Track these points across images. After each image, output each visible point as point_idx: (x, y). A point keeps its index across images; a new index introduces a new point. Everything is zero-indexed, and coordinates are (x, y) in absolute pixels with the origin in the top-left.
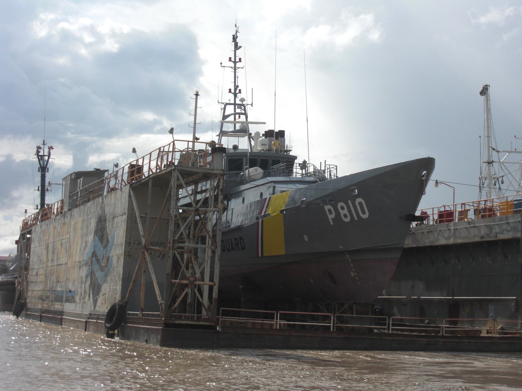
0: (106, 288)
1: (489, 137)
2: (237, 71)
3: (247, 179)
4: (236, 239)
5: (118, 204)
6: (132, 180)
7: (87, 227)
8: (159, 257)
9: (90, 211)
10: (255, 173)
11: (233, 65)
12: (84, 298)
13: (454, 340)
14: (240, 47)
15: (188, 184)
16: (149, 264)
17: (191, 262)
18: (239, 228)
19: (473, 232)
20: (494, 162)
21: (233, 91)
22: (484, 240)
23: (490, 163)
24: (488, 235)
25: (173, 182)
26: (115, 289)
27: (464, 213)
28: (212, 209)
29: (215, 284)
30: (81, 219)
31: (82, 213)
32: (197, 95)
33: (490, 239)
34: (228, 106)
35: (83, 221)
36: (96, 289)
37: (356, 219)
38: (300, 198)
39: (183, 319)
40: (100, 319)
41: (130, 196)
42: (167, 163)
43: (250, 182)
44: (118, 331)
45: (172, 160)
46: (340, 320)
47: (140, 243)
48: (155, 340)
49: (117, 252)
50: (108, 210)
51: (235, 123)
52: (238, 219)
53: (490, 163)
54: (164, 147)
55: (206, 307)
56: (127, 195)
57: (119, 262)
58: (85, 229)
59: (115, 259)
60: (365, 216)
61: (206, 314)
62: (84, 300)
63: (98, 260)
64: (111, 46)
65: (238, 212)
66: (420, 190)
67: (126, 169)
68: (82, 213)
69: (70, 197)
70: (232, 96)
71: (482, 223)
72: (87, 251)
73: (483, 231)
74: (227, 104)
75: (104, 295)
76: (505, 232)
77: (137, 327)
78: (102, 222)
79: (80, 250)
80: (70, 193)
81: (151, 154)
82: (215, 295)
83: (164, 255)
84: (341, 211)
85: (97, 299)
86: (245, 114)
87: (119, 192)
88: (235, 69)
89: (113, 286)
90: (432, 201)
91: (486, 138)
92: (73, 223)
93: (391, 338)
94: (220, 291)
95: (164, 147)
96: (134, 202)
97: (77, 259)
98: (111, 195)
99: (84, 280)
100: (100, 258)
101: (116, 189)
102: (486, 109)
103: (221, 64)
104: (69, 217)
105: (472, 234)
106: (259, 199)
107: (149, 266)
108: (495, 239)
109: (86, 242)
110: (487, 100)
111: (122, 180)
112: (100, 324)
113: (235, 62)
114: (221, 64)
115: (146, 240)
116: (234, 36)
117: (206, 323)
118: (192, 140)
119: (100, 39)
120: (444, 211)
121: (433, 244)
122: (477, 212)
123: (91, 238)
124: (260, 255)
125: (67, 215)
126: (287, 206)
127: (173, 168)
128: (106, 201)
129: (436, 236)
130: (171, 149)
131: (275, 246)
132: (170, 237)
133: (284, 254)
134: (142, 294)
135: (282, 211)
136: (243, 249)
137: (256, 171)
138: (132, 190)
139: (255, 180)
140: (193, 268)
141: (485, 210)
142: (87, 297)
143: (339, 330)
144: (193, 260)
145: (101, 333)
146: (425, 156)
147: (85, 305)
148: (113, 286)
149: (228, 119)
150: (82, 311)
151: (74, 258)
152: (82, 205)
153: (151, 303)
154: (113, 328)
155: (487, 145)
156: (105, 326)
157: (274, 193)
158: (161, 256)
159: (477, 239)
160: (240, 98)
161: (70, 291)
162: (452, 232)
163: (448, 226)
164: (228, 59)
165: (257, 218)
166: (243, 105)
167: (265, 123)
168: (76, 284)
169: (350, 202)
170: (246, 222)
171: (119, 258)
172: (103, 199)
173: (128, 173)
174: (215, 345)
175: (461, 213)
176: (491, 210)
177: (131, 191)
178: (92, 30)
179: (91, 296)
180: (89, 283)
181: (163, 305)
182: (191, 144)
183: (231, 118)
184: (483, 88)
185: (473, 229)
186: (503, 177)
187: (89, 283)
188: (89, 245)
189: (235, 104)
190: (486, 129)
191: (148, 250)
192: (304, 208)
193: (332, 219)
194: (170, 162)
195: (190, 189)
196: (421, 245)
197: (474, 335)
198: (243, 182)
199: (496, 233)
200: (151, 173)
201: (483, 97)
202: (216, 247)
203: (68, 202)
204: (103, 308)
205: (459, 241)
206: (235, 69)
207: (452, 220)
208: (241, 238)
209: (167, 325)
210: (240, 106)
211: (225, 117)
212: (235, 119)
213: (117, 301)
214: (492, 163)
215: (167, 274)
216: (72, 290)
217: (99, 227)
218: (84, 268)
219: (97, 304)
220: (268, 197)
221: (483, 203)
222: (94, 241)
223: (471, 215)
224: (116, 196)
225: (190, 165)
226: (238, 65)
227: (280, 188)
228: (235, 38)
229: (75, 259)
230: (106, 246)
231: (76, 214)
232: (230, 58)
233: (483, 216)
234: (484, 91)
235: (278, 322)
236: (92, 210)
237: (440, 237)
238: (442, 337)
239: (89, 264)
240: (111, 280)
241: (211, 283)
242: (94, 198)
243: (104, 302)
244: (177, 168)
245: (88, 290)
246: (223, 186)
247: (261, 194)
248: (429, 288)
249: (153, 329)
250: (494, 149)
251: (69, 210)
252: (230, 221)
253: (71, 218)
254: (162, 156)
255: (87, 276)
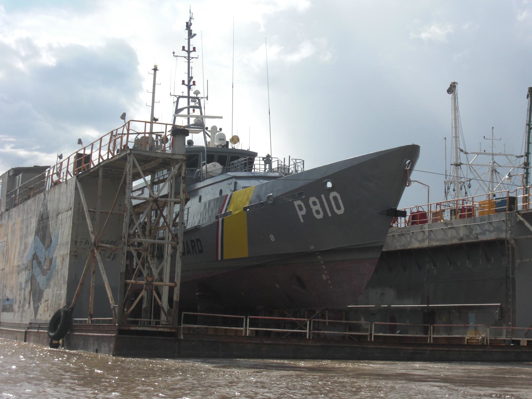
0: (48, 294)
1: (456, 137)
2: (191, 61)
3: (205, 176)
4: (192, 241)
5: (62, 200)
6: (79, 170)
7: (27, 227)
8: (109, 257)
9: (31, 209)
10: (213, 169)
11: (186, 55)
12: (24, 306)
13: (443, 349)
14: (195, 35)
15: (146, 173)
16: (99, 263)
17: (148, 262)
18: (196, 229)
19: (450, 233)
20: (462, 164)
21: (186, 83)
22: (463, 242)
23: (458, 165)
24: (468, 237)
25: (128, 167)
26: (60, 294)
27: (438, 215)
28: (173, 199)
29: (176, 285)
30: (19, 219)
31: (21, 212)
32: (155, 69)
33: (470, 241)
34: (181, 99)
35: (22, 221)
36: (37, 294)
37: (330, 215)
38: (266, 194)
39: (139, 324)
40: (42, 328)
41: (76, 188)
42: (121, 147)
43: (207, 179)
44: (63, 340)
45: (127, 144)
46: (316, 326)
47: (87, 242)
48: (107, 349)
49: (61, 253)
50: (51, 207)
51: (188, 117)
52: (195, 219)
53: (458, 165)
54: (117, 130)
55: (166, 310)
56: (73, 188)
57: (64, 264)
58: (24, 230)
59: (59, 261)
60: (341, 212)
61: (165, 320)
62: (24, 308)
63: (39, 263)
64: (48, 60)
65: (195, 213)
66: (404, 179)
67: (72, 160)
68: (21, 212)
69: (7, 196)
70: (185, 88)
71: (460, 224)
72: (26, 254)
73: (462, 233)
74: (180, 97)
75: (46, 301)
76: (487, 233)
77: (86, 335)
78: (44, 221)
79: (19, 253)
80: (8, 192)
81: (101, 139)
82: (176, 298)
83: (115, 255)
84: (312, 206)
85: (38, 307)
86: (200, 107)
87: (64, 185)
88: (189, 58)
89: (57, 291)
90: (410, 200)
91: (454, 139)
92: (11, 224)
93: (373, 346)
94: (181, 295)
95: (117, 130)
96: (81, 194)
97: (16, 264)
98: (55, 190)
99: (23, 286)
100: (42, 260)
101: (60, 182)
102: (453, 108)
103: (174, 53)
104: (7, 218)
105: (450, 237)
106: (218, 196)
107: (100, 266)
108: (477, 240)
109: (26, 244)
110: (455, 99)
111: (68, 172)
112: (42, 335)
113: (189, 52)
114: (174, 53)
115: (96, 237)
116: (187, 23)
117: (166, 330)
118: (149, 121)
119: (35, 52)
120: (417, 212)
121: (405, 248)
122: (453, 212)
123: (31, 239)
124: (220, 258)
125: (4, 215)
126: (251, 203)
127: (129, 152)
128: (48, 197)
129: (408, 239)
130: (125, 131)
131: (236, 247)
132: (125, 231)
133: (246, 255)
134: (91, 298)
135: (245, 209)
136: (201, 251)
137: (215, 167)
138: (80, 181)
139: (213, 177)
140: (149, 268)
141: (463, 210)
142: (27, 305)
143: (317, 337)
144: (149, 259)
145: (43, 344)
146: (410, 143)
147: (24, 314)
148: (57, 291)
149: (181, 113)
150: (21, 321)
151: (12, 262)
152: (21, 203)
153: (102, 306)
154: (57, 338)
155: (454, 146)
156: (49, 335)
157: (235, 190)
158: (112, 257)
159: (455, 241)
160: (194, 91)
161: (8, 300)
162: (427, 234)
163: (422, 228)
164: (182, 48)
165: (217, 217)
166: (198, 98)
167: (221, 118)
168: (14, 291)
169: (323, 196)
170: (204, 222)
171: (63, 259)
172: (45, 195)
173: (74, 163)
174: (176, 355)
175: (435, 214)
176: (470, 209)
177: (78, 183)
178: (28, 43)
179: (32, 303)
180: (28, 289)
181: (117, 310)
182: (148, 125)
183: (185, 112)
184: (451, 85)
185: (450, 230)
186: (470, 180)
187: (30, 289)
188: (30, 246)
189: (188, 97)
190: (454, 129)
191: (98, 247)
192: (271, 204)
193: (302, 216)
194: (124, 146)
195: (148, 178)
196: (391, 249)
197: (459, 343)
198: (199, 180)
199: (477, 235)
200: (101, 161)
201: (451, 95)
202: (178, 243)
203: (5, 201)
204: (45, 316)
205: (435, 244)
206: (189, 58)
207: (426, 222)
208: (198, 240)
209: (121, 332)
210: (194, 99)
211: (178, 111)
212: (189, 113)
213: (61, 307)
214: (460, 165)
215: (121, 273)
216: (10, 297)
217: (41, 226)
218: (24, 272)
219: (39, 312)
220: (230, 194)
221: (461, 202)
222: (35, 241)
223: (447, 216)
224: (60, 190)
225: (148, 149)
226: (192, 55)
227: (241, 183)
228: (188, 26)
229: (13, 263)
230: (49, 246)
231: (14, 214)
232: (184, 47)
233: (461, 217)
234: (452, 89)
235: (247, 330)
236: (33, 208)
237: (413, 240)
238: (430, 345)
239: (29, 268)
240: (55, 284)
241: (171, 284)
242: (34, 195)
243: (46, 309)
244: (132, 151)
245: (27, 297)
246: (185, 174)
247: (221, 191)
248: (401, 295)
249: (105, 336)
250: (462, 151)
251: (7, 210)
252: (185, 222)
253: (8, 218)
254: (115, 140)
255: (27, 282)
